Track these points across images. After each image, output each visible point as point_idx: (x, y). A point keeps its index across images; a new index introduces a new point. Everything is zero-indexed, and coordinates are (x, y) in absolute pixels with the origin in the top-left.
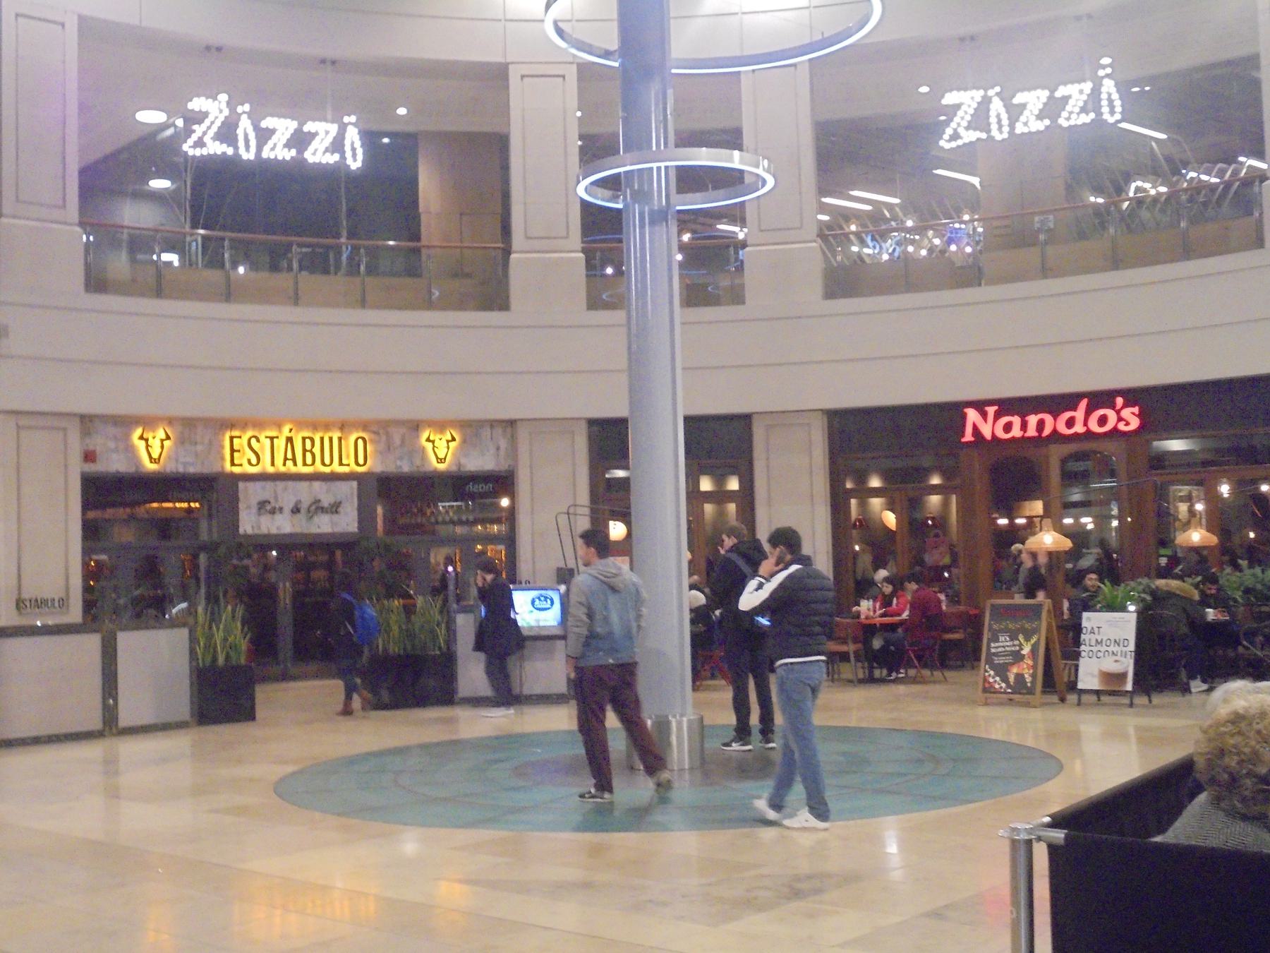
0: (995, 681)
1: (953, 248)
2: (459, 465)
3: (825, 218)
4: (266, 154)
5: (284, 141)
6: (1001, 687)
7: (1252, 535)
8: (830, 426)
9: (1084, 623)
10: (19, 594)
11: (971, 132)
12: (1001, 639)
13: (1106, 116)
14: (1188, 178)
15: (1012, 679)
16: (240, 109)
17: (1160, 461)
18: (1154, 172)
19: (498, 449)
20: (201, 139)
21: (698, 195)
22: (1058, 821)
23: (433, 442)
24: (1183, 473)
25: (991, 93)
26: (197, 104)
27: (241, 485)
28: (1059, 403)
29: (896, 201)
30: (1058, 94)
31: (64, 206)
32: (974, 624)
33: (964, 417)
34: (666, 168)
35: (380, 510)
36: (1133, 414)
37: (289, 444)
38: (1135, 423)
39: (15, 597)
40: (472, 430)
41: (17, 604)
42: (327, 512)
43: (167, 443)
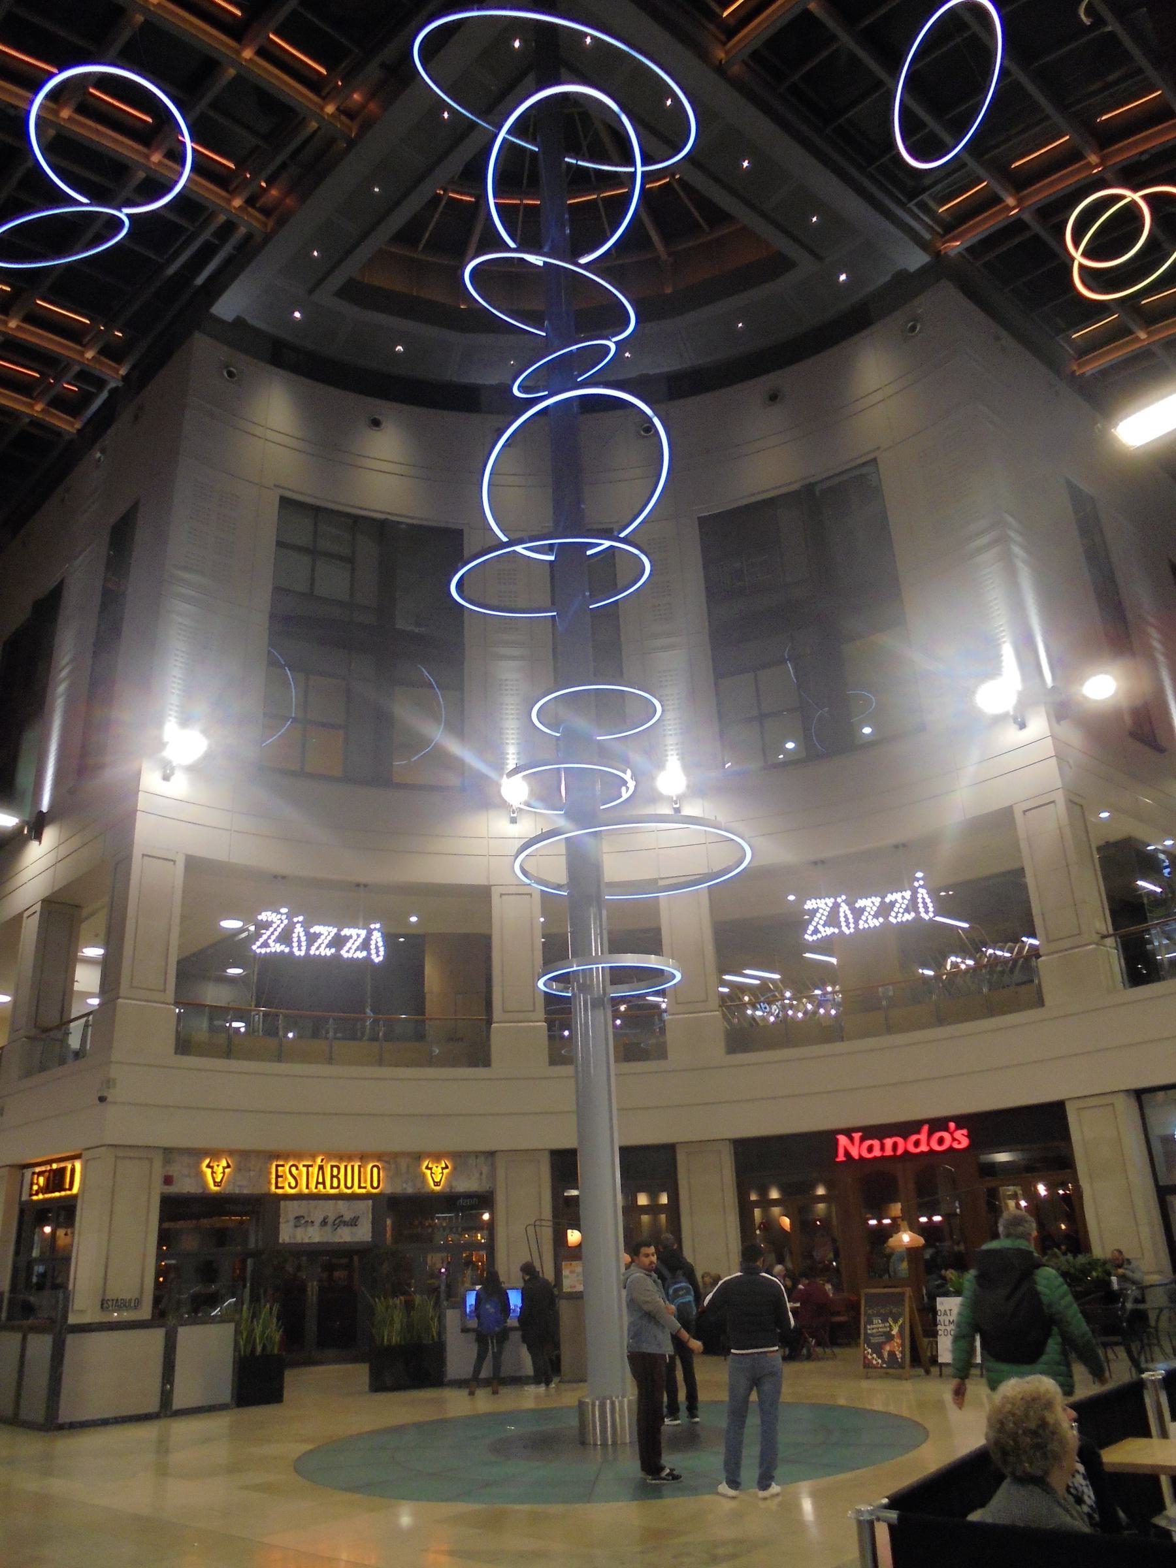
0: (873, 1358)
1: (822, 1011)
2: (451, 1187)
3: (726, 990)
5: (326, 942)
7: (1063, 1227)
8: (735, 1148)
9: (939, 1307)
10: (104, 1291)
11: (827, 928)
12: (875, 1321)
13: (923, 915)
14: (988, 954)
15: (886, 1355)
16: (295, 920)
17: (992, 1170)
18: (964, 952)
19: (481, 1174)
20: (266, 941)
21: (625, 986)
22: (895, 1502)
23: (431, 1169)
25: (839, 900)
26: (264, 916)
28: (906, 1129)
29: (777, 976)
30: (887, 900)
31: (164, 991)
32: (854, 1307)
34: (602, 967)
35: (389, 1222)
36: (963, 1134)
37: (321, 1172)
38: (965, 1143)
39: (101, 1298)
40: (460, 1159)
41: (102, 1304)
42: (348, 1225)
43: (227, 1170)
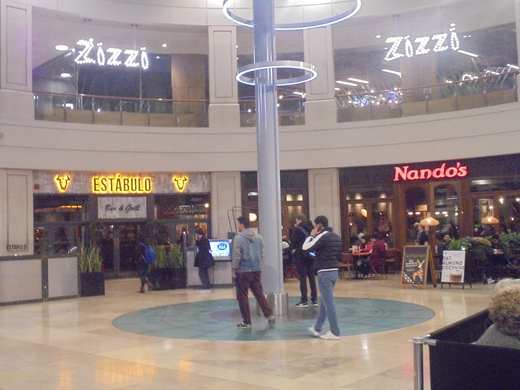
0: (408, 279)
1: (390, 101)
2: (188, 190)
3: (338, 89)
4: (109, 63)
5: (116, 58)
6: (410, 281)
7: (513, 219)
8: (340, 175)
9: (444, 255)
10: (8, 243)
11: (398, 54)
12: (410, 261)
13: (453, 48)
14: (486, 73)
15: (414, 278)
16: (98, 45)
17: (475, 189)
18: (472, 70)
19: (204, 184)
20: (82, 57)
21: (286, 80)
23: (177, 181)
24: (485, 193)
25: (406, 38)
26: (81, 43)
27: (99, 198)
28: (433, 165)
29: (367, 82)
30: (433, 39)
31: (26, 84)
32: (399, 255)
33: (395, 170)
34: (273, 69)
35: (155, 209)
36: (464, 169)
37: (118, 182)
38: (465, 173)
39: (6, 244)
40: (193, 176)
41: (7, 247)
42: (134, 210)
43: (68, 181)
